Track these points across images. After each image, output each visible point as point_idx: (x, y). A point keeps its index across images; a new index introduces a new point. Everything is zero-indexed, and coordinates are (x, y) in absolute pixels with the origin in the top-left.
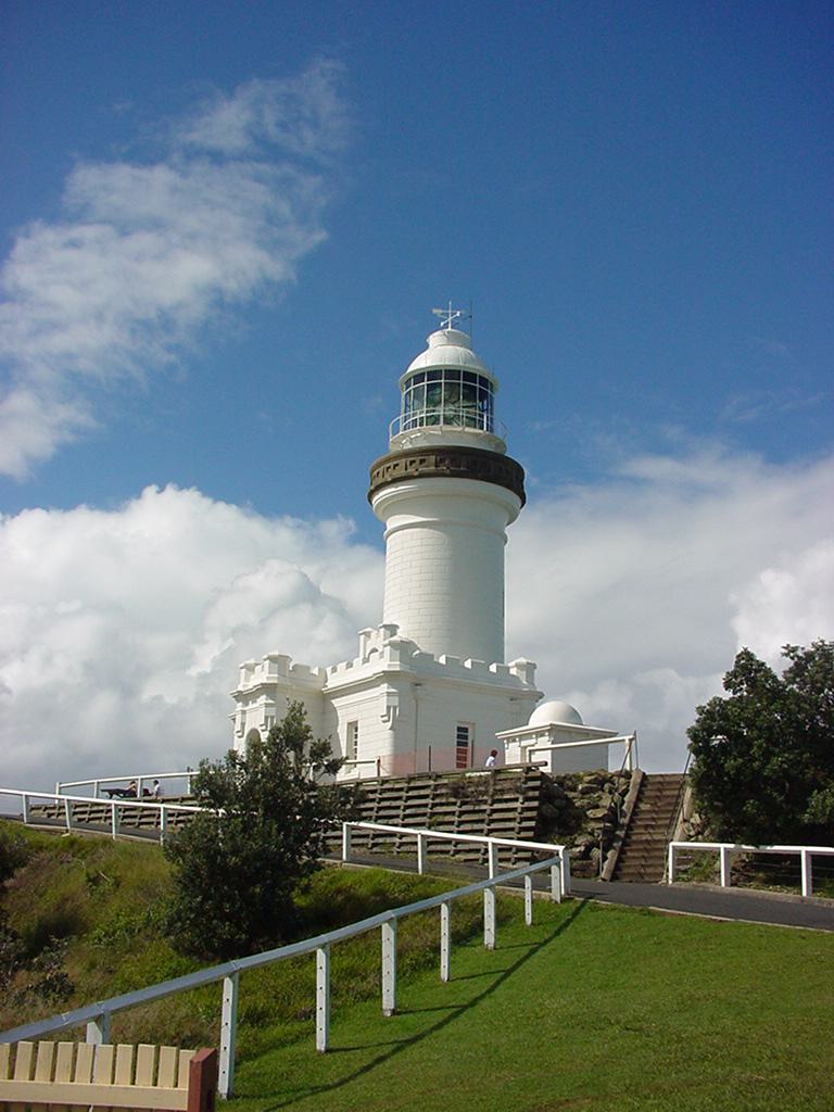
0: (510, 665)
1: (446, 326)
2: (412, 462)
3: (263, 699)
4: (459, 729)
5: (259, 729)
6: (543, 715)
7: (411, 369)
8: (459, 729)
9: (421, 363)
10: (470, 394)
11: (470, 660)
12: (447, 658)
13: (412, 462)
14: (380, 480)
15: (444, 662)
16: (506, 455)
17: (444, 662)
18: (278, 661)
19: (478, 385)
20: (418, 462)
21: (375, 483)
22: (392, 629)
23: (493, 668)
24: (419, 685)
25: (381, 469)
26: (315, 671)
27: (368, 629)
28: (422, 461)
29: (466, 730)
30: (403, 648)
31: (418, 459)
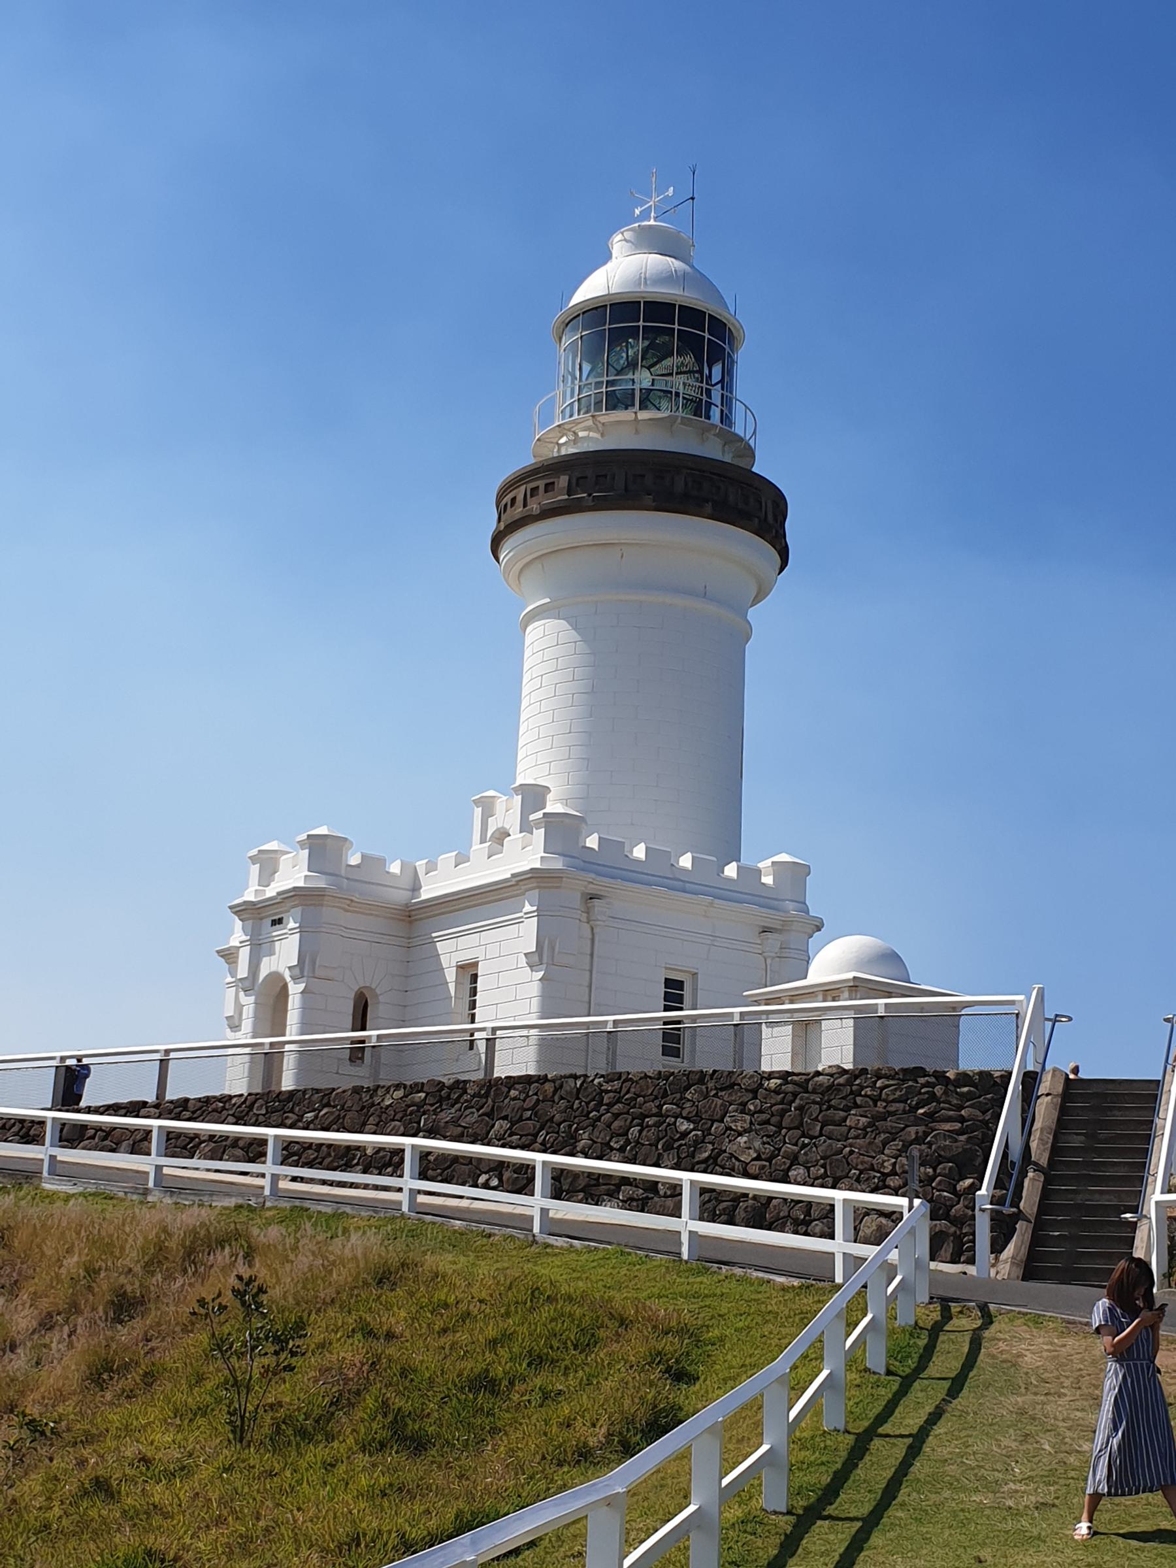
0: (760, 865)
1: (645, 215)
2: (534, 491)
3: (825, 1513)
4: (669, 983)
5: (287, 976)
6: (831, 961)
7: (574, 302)
8: (669, 983)
9: (594, 286)
10: (691, 344)
11: (689, 855)
12: (647, 848)
13: (534, 491)
14: (518, 511)
15: (596, 847)
16: (754, 470)
17: (596, 847)
18: (321, 850)
19: (707, 335)
20: (542, 489)
21: (508, 518)
22: (533, 796)
23: (731, 871)
24: (598, 897)
25: (520, 493)
26: (395, 868)
27: (491, 793)
28: (549, 487)
29: (679, 985)
30: (561, 831)
31: (541, 484)
